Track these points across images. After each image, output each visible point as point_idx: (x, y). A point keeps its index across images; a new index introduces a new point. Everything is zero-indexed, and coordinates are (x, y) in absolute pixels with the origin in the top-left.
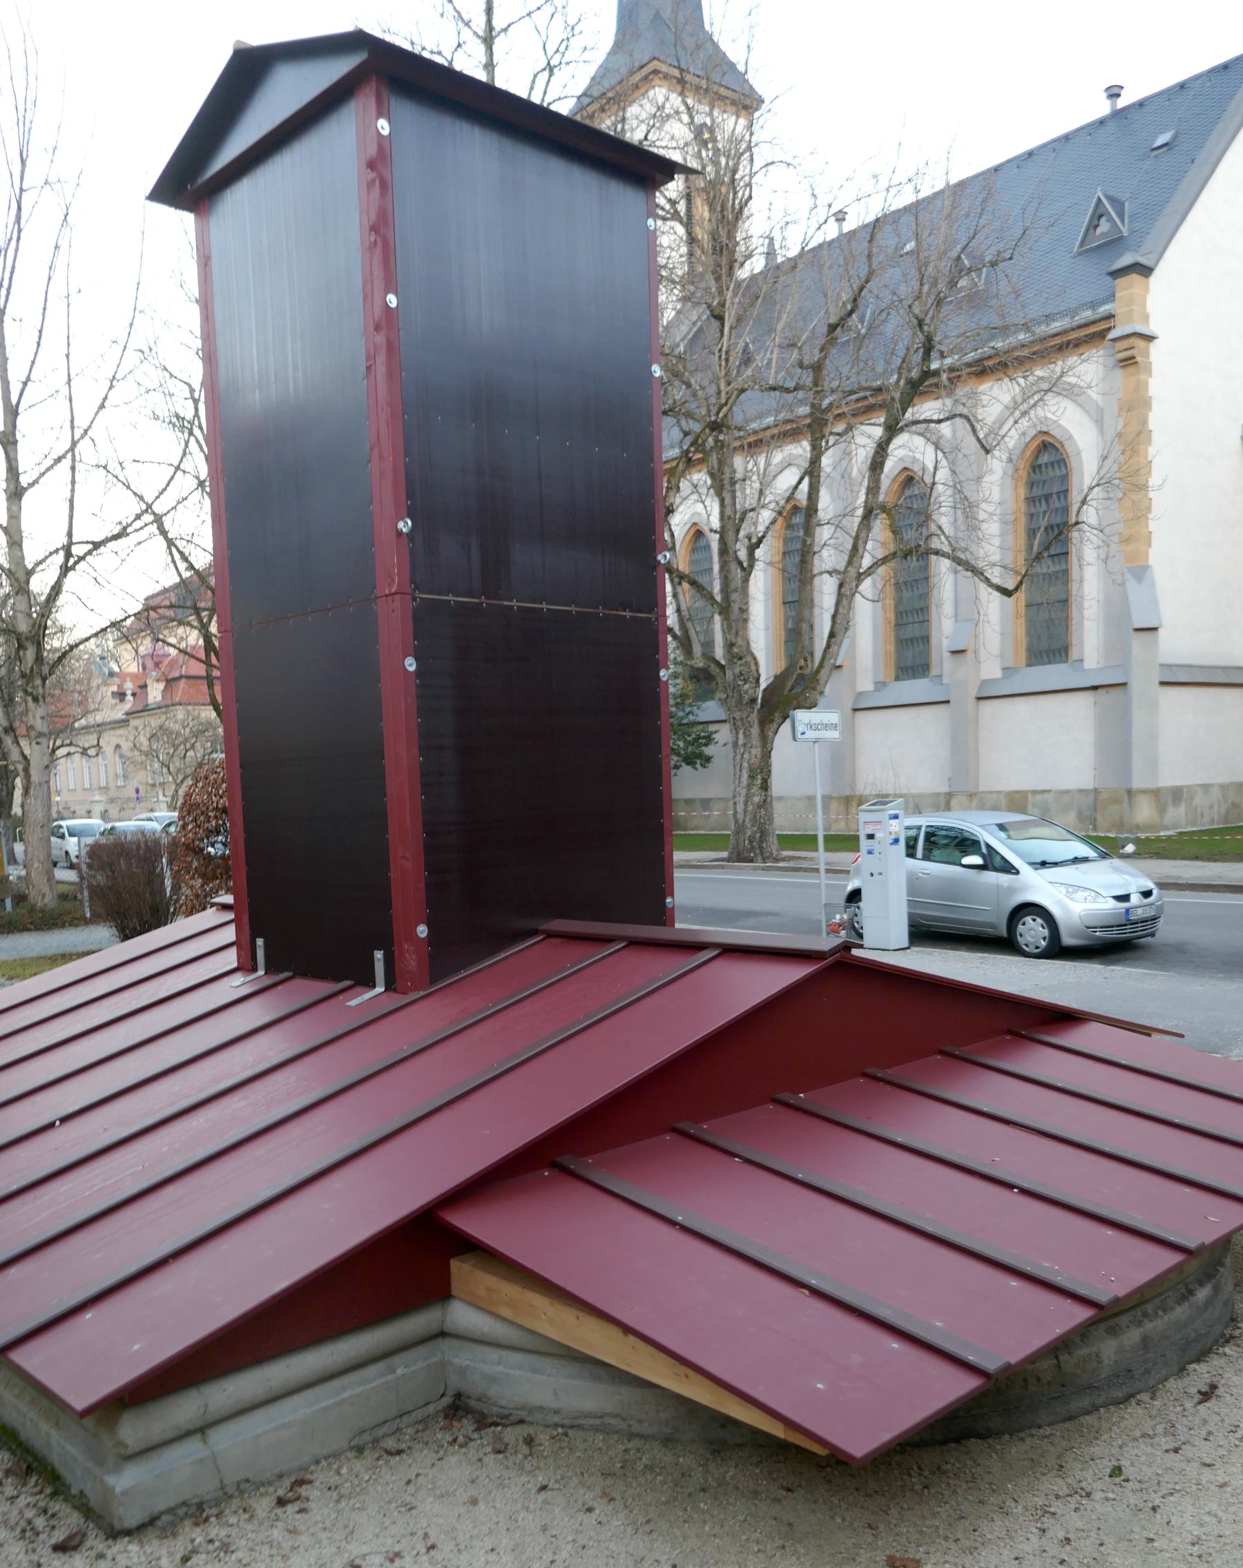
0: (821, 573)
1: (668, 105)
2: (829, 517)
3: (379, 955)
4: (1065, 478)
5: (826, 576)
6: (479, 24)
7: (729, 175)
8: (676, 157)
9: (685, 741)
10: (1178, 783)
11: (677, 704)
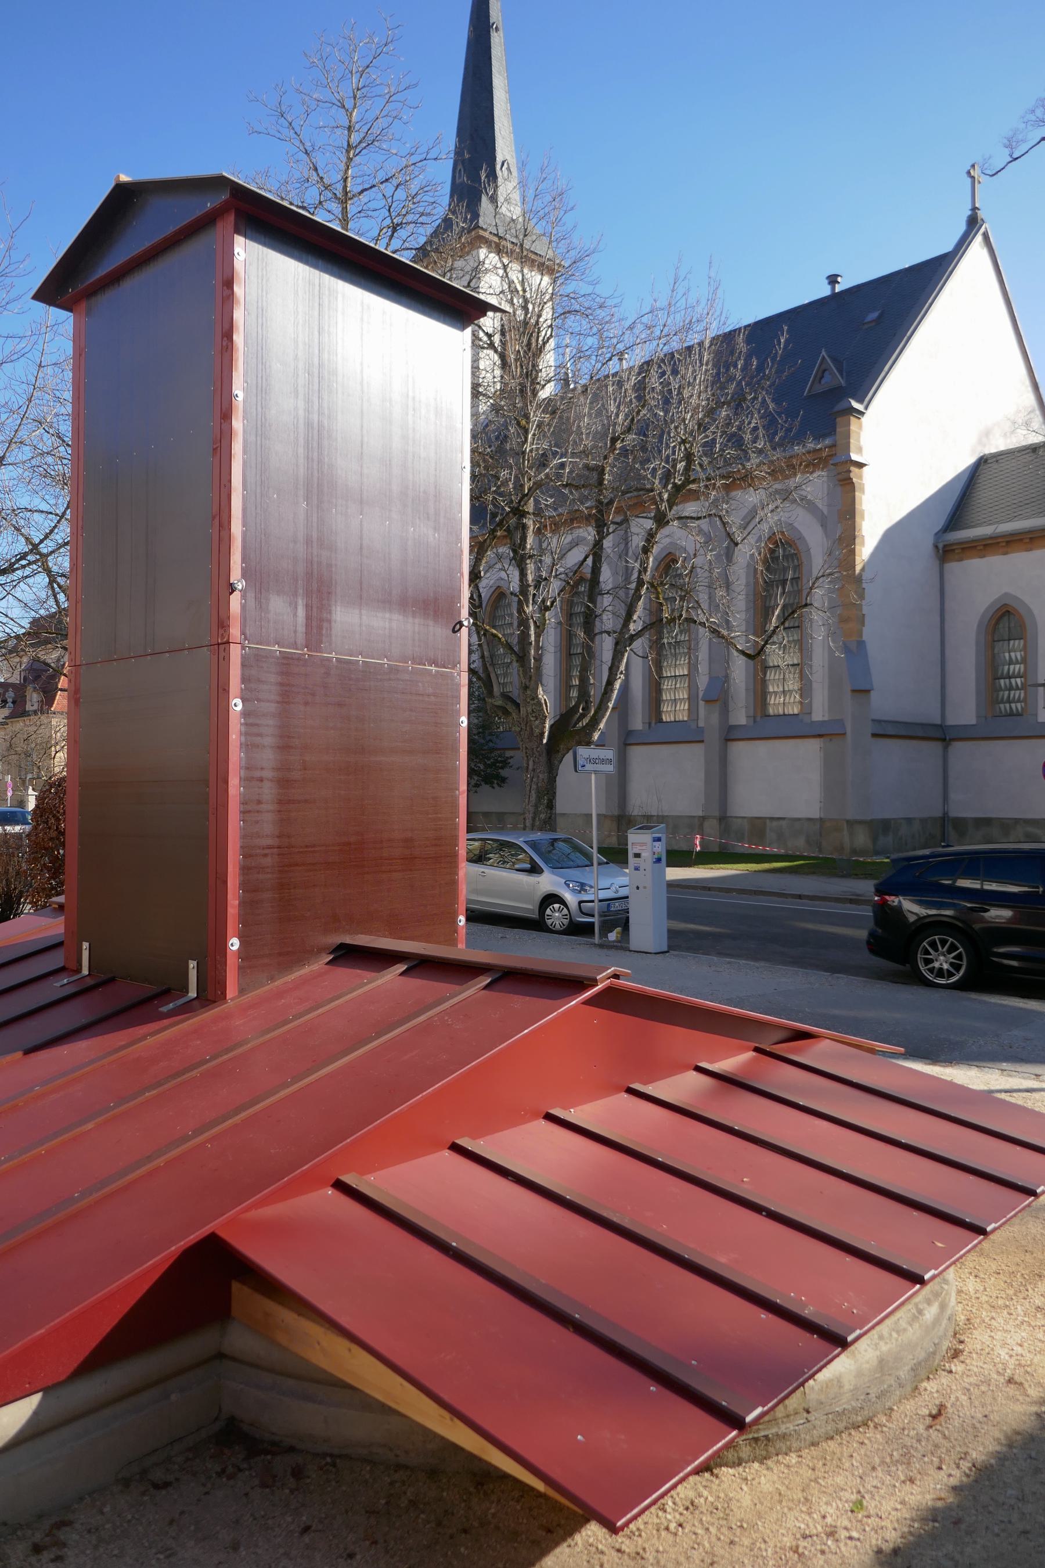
0: (601, 633)
1: (487, 262)
2: (608, 588)
3: (192, 964)
4: (798, 568)
5: (605, 635)
6: (339, 190)
7: (535, 318)
8: (493, 300)
9: (485, 764)
10: (887, 815)
11: (479, 733)
